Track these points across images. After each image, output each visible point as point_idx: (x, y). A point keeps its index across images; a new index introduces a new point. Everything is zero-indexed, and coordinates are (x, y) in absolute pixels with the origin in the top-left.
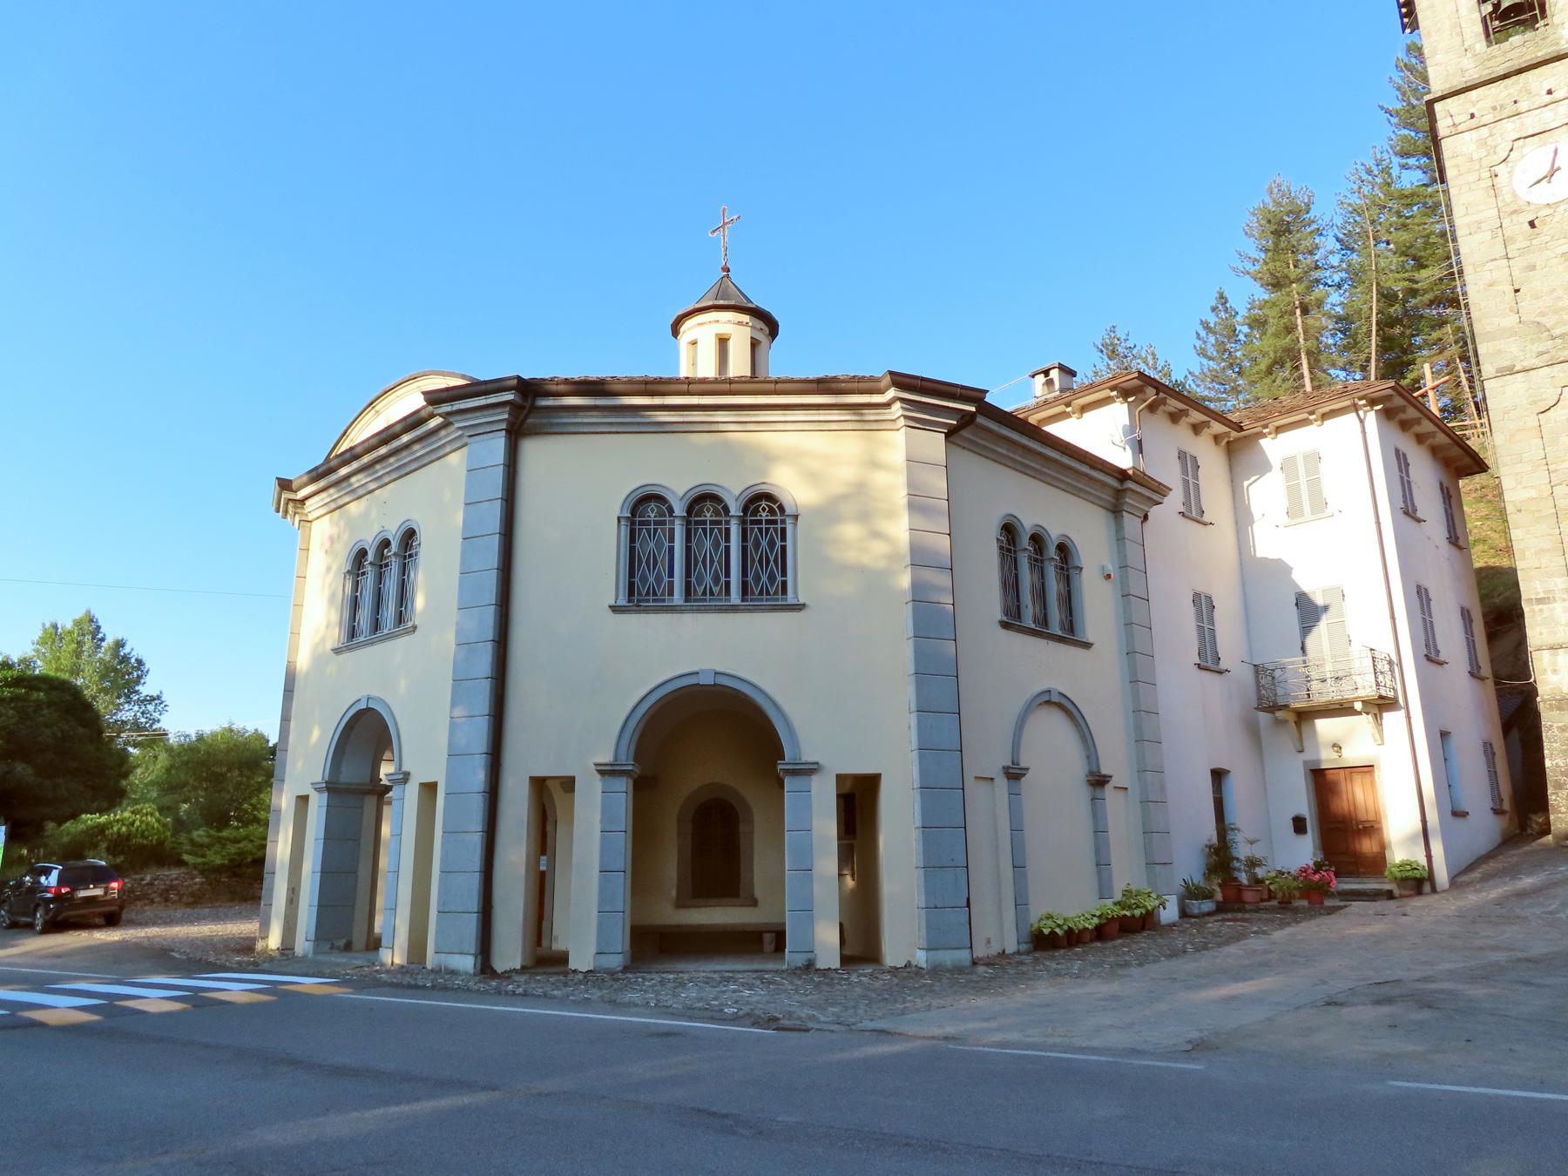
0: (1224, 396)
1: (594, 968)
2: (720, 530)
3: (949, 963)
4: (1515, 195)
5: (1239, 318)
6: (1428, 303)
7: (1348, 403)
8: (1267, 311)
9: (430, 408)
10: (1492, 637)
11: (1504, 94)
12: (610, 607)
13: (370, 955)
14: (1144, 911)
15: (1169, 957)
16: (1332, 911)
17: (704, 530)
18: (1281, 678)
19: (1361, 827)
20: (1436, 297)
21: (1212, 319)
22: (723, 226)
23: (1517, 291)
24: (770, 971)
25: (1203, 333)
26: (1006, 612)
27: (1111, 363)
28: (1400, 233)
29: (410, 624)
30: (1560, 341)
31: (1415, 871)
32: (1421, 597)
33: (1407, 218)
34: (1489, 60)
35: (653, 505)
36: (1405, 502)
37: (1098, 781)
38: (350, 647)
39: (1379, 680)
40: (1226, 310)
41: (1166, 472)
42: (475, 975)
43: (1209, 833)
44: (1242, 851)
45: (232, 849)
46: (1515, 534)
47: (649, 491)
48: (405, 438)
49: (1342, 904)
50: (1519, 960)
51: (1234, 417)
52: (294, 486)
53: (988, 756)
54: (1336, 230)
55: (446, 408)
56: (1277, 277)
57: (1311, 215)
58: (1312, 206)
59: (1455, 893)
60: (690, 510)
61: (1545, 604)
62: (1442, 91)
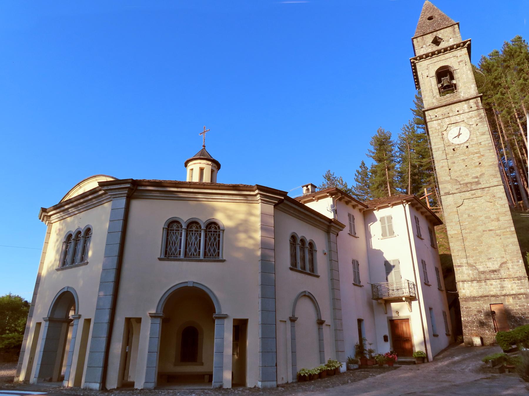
0: (364, 194)
1: (144, 388)
2: (198, 234)
3: (269, 387)
4: (449, 141)
5: (368, 170)
6: (426, 169)
7: (400, 201)
8: (377, 169)
9: (100, 188)
10: (445, 277)
11: (445, 111)
12: (158, 258)
13: (59, 383)
14: (335, 368)
15: (343, 384)
16: (396, 368)
17: (192, 233)
18: (380, 289)
19: (405, 339)
20: (428, 168)
21: (360, 170)
22: (204, 132)
23: (450, 169)
24: (207, 389)
25: (357, 174)
26: (292, 264)
27: (328, 182)
28: (417, 147)
29: (86, 261)
30: (463, 185)
31: (422, 355)
32: (423, 264)
33: (419, 143)
34: (441, 100)
35: (175, 224)
36: (418, 233)
37: (320, 323)
38: (63, 269)
39: (410, 290)
40: (364, 167)
41: (344, 220)
42: (99, 390)
43: (357, 341)
44: (368, 347)
45: (6, 342)
46: (451, 245)
47: (175, 219)
48: (90, 197)
49: (399, 366)
50: (453, 385)
51: (365, 203)
52: (47, 211)
53: (284, 314)
54: (398, 145)
55: (105, 188)
56: (380, 158)
57: (391, 140)
58: (391, 137)
59: (434, 362)
60: (188, 227)
61: (460, 267)
62: (427, 108)
